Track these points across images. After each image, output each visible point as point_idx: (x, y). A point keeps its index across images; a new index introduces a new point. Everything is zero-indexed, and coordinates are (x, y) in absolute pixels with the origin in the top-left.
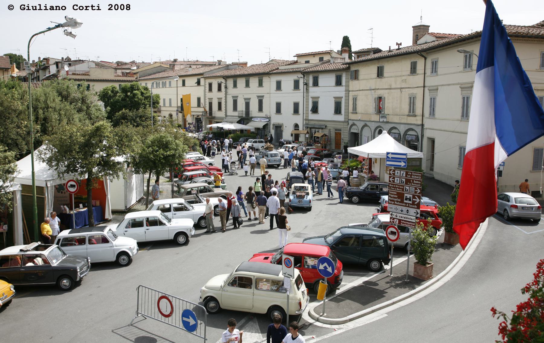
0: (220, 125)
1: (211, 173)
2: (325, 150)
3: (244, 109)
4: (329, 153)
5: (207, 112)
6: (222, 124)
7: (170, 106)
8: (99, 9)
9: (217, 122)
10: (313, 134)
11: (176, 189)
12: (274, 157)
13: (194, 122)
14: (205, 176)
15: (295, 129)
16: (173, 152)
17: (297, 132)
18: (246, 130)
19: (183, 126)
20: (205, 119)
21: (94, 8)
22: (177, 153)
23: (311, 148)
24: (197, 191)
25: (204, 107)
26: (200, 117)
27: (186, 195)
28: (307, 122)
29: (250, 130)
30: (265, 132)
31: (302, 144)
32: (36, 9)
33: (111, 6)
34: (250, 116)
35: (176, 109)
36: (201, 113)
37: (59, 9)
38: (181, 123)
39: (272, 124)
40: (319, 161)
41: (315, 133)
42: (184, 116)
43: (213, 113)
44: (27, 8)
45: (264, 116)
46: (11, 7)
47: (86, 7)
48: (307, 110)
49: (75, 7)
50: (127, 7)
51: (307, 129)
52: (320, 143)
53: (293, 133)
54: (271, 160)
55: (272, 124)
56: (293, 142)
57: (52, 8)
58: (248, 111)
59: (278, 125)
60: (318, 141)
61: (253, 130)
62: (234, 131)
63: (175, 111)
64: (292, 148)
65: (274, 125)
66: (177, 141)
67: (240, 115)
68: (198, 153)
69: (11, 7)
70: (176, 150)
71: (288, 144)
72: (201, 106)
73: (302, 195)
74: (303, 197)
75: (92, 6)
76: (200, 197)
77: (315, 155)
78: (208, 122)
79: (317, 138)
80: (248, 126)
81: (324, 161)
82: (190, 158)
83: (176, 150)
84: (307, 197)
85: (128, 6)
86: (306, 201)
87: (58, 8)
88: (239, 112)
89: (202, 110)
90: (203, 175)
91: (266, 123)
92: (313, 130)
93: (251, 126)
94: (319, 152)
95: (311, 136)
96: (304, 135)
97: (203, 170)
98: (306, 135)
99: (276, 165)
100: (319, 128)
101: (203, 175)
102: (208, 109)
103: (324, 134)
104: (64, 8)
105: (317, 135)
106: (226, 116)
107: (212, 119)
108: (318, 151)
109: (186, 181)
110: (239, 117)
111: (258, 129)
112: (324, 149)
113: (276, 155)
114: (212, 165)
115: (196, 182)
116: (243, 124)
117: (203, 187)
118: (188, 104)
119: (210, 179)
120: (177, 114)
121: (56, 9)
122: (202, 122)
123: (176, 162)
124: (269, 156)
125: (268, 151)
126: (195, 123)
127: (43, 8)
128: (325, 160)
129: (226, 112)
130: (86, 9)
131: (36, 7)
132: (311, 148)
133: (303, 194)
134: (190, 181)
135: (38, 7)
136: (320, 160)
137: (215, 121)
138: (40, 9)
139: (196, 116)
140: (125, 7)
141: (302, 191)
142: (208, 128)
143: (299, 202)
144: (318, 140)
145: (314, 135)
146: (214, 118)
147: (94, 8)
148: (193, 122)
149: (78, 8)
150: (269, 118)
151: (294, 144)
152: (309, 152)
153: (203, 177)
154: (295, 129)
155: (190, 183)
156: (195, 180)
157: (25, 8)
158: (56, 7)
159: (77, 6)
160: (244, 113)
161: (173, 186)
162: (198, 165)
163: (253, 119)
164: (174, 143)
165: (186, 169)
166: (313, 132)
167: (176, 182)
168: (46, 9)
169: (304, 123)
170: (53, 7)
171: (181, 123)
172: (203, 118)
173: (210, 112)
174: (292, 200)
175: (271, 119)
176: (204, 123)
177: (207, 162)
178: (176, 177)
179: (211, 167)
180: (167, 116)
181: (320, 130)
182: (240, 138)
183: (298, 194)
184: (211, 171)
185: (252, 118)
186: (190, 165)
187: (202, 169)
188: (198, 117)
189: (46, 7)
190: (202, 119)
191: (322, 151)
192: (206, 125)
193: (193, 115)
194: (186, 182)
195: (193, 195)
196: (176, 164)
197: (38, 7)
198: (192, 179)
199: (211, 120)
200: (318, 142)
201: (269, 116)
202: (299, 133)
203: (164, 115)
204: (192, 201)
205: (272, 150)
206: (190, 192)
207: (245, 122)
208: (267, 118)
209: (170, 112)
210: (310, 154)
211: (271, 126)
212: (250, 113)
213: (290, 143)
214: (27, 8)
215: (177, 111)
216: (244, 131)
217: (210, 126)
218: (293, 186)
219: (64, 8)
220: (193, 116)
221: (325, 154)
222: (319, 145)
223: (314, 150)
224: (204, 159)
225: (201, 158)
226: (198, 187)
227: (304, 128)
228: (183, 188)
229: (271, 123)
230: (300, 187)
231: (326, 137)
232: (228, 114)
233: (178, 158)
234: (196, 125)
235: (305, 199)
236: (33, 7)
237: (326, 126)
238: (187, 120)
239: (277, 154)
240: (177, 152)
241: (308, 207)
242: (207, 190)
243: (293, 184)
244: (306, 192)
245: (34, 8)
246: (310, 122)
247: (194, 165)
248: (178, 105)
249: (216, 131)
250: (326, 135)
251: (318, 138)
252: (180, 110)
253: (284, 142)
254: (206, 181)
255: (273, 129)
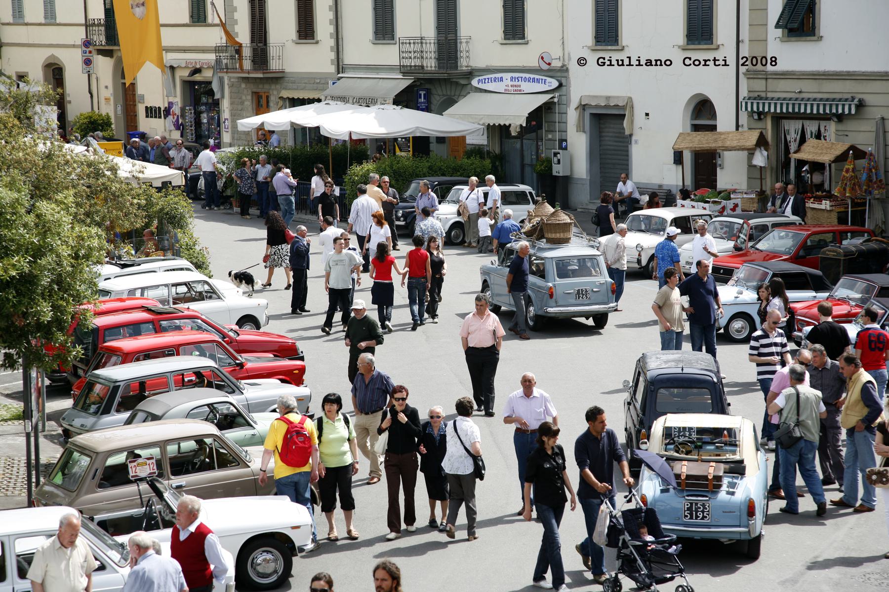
0: (306, 116)
1: (241, 365)
2: (855, 234)
3: (430, 31)
4: (873, 245)
5: (239, 50)
6: (319, 113)
7: (50, 18)
8: (726, 65)
9: (295, 102)
10: (793, 147)
11: (51, 453)
12: (575, 274)
13: (178, 100)
14: (210, 385)
15: (696, 128)
16: (20, 263)
17: (704, 141)
18: (441, 140)
19: (117, 127)
20: (231, 86)
21: (717, 63)
22: (43, 268)
23: (776, 225)
24: (159, 464)
25: (223, 25)
26: (207, 74)
27: (101, 486)
28: (759, 85)
29: (463, 138)
30: (542, 148)
31: (730, 204)
32: (623, 65)
33: (745, 59)
34: (464, 64)
35: (79, 35)
36: (212, 57)
37: (661, 65)
38: (109, 108)
39: (574, 103)
40: (817, 289)
41: (803, 140)
42: (120, 72)
43: (273, 52)
44: (608, 63)
45: (534, 63)
46: (582, 62)
47: (705, 61)
48: (759, 24)
49: (687, 62)
50: (772, 61)
51: (760, 125)
52: (829, 196)
53: (680, 146)
54: (558, 292)
55: (574, 103)
56: (685, 195)
57: (649, 63)
58: (451, 37)
59: (607, 107)
60: (820, 187)
61: (477, 139)
62: (385, 145)
63: (74, 46)
64: (677, 222)
65: (583, 107)
66: (44, 206)
67: (407, 62)
68: (184, 263)
69: (582, 62)
70: (38, 252)
71: (657, 206)
72: (210, 20)
73: (705, 478)
74: (711, 485)
75: (715, 60)
76: (166, 495)
77: (795, 259)
78: (248, 103)
79: (811, 171)
80: (450, 115)
81: (841, 292)
82: (143, 289)
83: (38, 252)
84: (732, 485)
85: (773, 59)
86: (728, 510)
87: (659, 63)
88: (406, 47)
89: (214, 37)
90: (201, 379)
91: (545, 98)
92: (792, 128)
93: (464, 117)
94: (822, 244)
95: (782, 164)
96: (746, 153)
97: (202, 354)
98: (751, 152)
99: (587, 315)
100: (826, 117)
101: (201, 379)
102: (243, 35)
103: (852, 147)
104: (668, 63)
105: (811, 152)
106: (340, 67)
107: (267, 86)
108: (817, 238)
109: (107, 411)
110: (405, 71)
111: (500, 131)
112: (850, 227)
113: (584, 265)
114: (258, 326)
115: (155, 418)
116: (427, 109)
117: (192, 445)
118: (138, 11)
119: (232, 398)
120: (88, 62)
121: (656, 65)
122: (216, 104)
123: (38, 313)
124: (552, 270)
125: (543, 243)
126: (183, 110)
127: (634, 62)
128: (851, 288)
129: (338, 49)
130: (705, 65)
131: (622, 61)
132: (776, 225)
133: (711, 470)
134: (126, 415)
135: (626, 62)
136: (818, 285)
137: (285, 94)
138: (630, 65)
139: (185, 73)
140: (769, 61)
141: (709, 453)
142: (247, 133)
143: (692, 511)
144: (817, 178)
145: (794, 157)
146: (278, 79)
147: (717, 63)
148: (171, 104)
149: (691, 62)
150: (560, 73)
151: (687, 202)
152: (762, 245)
153: (197, 390)
154: (696, 128)
155: (129, 422)
156: (154, 404)
157: (604, 63)
158: (656, 61)
159: (690, 59)
160: (431, 48)
161: (32, 438)
162: (178, 328)
163: (474, 82)
164: (30, 219)
165: (114, 351)
166: (793, 137)
167: (56, 416)
168: (639, 65)
169: (744, 93)
170: (651, 61)
171: (109, 108)
172: (221, 81)
173: (254, 51)
174: (655, 500)
175: (567, 78)
176: (226, 106)
177: (230, 310)
178: (58, 390)
179: (248, 335)
180: (36, 74)
181: (831, 128)
182: (410, 182)
183: (685, 468)
184: (242, 358)
185: (471, 74)
186: (135, 329)
187: (197, 346)
188: (197, 77)
189: (639, 61)
190: (215, 86)
191: (839, 236)
192: (237, 115)
193: (172, 68)
194: (107, 419)
195: (132, 489)
196: (46, 330)
197: (626, 62)
198: (141, 397)
199: (260, 89)
200: (821, 192)
201: (556, 64)
202: (713, 145)
203: (22, 69)
204: (131, 518)
205: (566, 241)
206: (122, 469)
207: (436, 100)
208: (551, 72)
209: (48, 52)
210: (771, 256)
211: (572, 116)
212: (462, 47)
213: (669, 201)
214: (608, 63)
215: (87, 43)
216: (433, 146)
217: (255, 121)
218: (658, 427)
219: (668, 63)
220: (168, 71)
221: (848, 253)
222: (826, 205)
223: (791, 232)
224: (212, 294)
225: (199, 288)
226: (162, 444)
227: (744, 118)
228: (84, 450)
229: (568, 95)
230: (701, 431)
231: (862, 163)
232: (350, 57)
233: (49, 294)
234: (190, 117)
235: (722, 495)
236: (617, 61)
237: (861, 105)
238: (140, 90)
239: (592, 258)
240: (43, 262)
241: (739, 542)
242: (211, 456)
243: (661, 420)
244: (730, 457)
245: (620, 63)
246: (773, 84)
247: (158, 330)
248: (91, 16)
249: (290, 143)
250: (859, 154)
251: (817, 167)
252: (100, 38)
253: (636, 195)
254: (212, 413)
255: (580, 128)
